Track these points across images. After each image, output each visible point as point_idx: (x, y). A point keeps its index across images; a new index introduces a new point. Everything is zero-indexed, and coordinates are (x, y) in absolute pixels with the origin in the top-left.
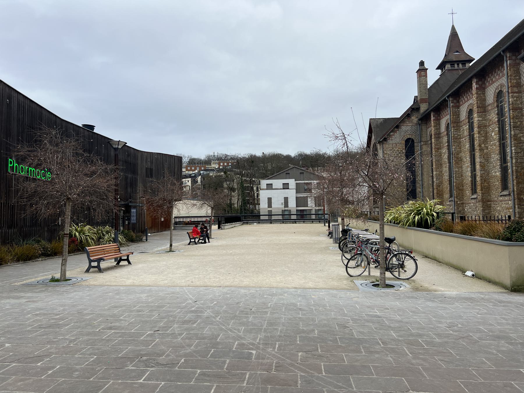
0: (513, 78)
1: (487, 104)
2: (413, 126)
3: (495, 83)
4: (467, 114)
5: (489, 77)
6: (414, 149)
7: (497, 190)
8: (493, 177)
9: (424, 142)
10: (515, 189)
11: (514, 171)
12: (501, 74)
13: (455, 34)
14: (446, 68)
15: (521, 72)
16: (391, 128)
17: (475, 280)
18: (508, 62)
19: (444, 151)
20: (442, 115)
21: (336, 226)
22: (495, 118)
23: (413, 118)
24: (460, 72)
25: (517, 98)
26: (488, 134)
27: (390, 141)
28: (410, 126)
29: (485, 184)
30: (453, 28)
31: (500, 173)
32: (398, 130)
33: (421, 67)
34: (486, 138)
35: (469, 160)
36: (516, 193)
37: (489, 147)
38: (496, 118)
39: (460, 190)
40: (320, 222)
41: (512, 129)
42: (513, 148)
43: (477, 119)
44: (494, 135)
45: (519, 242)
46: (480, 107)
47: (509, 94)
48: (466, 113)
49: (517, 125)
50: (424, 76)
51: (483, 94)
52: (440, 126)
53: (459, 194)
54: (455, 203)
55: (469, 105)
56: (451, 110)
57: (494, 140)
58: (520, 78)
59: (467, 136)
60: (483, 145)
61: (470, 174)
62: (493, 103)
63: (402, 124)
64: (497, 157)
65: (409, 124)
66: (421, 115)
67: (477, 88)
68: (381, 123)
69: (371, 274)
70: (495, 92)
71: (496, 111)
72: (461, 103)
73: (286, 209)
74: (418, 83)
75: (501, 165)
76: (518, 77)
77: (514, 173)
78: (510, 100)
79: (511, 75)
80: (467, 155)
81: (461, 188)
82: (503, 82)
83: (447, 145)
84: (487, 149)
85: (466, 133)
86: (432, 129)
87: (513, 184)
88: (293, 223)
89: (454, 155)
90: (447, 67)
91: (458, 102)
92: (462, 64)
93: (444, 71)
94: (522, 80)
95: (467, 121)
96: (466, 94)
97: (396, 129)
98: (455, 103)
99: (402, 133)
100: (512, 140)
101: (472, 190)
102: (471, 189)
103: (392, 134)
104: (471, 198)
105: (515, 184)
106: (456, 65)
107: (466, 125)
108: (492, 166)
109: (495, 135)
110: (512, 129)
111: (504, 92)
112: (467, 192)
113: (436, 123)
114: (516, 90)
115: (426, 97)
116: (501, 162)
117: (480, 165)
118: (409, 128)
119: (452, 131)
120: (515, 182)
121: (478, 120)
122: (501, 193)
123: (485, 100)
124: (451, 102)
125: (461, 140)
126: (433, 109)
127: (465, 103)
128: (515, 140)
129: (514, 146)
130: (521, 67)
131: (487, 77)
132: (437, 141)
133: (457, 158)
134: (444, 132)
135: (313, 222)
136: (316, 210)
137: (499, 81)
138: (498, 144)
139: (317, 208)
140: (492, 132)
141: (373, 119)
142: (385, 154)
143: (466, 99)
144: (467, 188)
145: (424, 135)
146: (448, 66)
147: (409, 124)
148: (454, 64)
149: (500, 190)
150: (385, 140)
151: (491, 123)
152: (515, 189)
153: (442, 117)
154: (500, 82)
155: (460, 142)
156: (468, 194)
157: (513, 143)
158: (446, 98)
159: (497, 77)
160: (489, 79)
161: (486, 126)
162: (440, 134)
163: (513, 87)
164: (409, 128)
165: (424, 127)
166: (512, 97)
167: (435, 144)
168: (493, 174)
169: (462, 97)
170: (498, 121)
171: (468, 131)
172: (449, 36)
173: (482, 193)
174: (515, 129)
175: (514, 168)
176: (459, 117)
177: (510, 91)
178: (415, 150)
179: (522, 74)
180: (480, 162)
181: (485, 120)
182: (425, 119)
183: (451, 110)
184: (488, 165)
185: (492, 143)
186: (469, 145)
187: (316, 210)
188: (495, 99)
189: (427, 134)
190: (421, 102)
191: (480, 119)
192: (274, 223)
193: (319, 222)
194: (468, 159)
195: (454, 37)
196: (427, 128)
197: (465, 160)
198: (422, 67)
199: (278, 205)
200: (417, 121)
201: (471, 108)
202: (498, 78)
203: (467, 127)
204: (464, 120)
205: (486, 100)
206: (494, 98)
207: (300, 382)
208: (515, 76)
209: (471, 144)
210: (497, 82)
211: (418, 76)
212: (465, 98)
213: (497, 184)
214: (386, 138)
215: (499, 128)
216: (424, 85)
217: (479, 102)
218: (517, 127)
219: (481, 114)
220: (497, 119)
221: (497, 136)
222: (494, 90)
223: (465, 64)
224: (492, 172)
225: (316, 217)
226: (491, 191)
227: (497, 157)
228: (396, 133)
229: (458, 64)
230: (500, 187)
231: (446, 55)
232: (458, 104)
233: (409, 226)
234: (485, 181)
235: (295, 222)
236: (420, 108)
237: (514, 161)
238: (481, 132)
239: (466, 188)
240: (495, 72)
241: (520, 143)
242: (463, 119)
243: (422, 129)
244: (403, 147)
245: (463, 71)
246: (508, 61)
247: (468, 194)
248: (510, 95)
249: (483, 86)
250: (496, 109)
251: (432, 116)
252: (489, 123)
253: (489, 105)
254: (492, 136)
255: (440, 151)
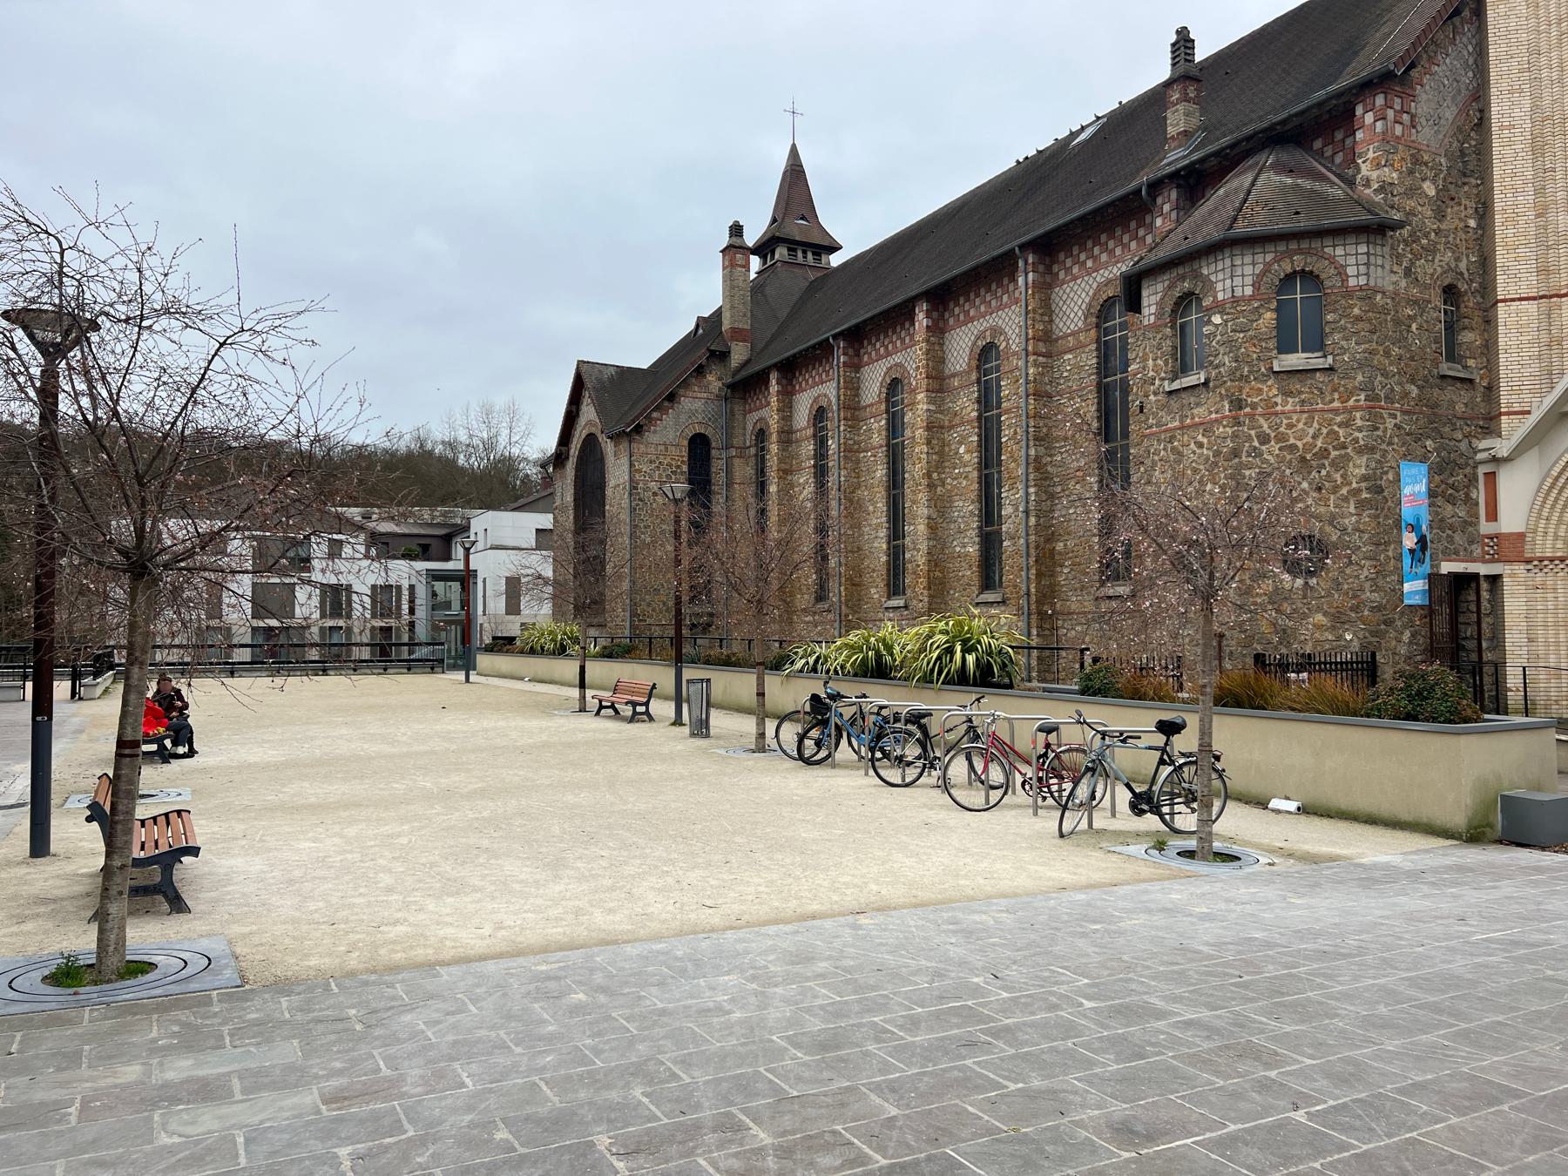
0: (1038, 317)
1: (947, 371)
2: (709, 402)
3: (975, 323)
4: (884, 390)
5: (957, 304)
6: (709, 466)
7: (964, 590)
8: (956, 555)
9: (737, 448)
10: (1033, 590)
11: (1032, 545)
12: (994, 303)
13: (798, 168)
14: (777, 256)
15: (1054, 306)
16: (655, 400)
17: (1303, 818)
18: (1031, 275)
19: (801, 481)
20: (800, 384)
21: (705, 685)
22: (969, 409)
23: (710, 378)
24: (812, 276)
25: (1043, 367)
26: (947, 449)
27: (651, 435)
28: (703, 401)
29: (937, 573)
30: (794, 152)
31: (977, 547)
32: (672, 408)
33: (734, 239)
34: (941, 458)
35: (885, 509)
36: (1033, 598)
37: (949, 480)
38: (973, 410)
39: (853, 585)
40: (409, 669)
41: (1031, 443)
42: (1032, 490)
43: (925, 407)
44: (966, 453)
45: (1440, 722)
46: (932, 378)
47: (1027, 355)
48: (881, 386)
49: (1042, 435)
50: (744, 266)
51: (939, 344)
52: (791, 412)
53: (852, 594)
54: (843, 618)
55: (891, 367)
56: (842, 373)
57: (965, 466)
58: (1051, 321)
59: (881, 446)
60: (935, 475)
61: (885, 546)
62: (968, 373)
63: (682, 391)
64: (971, 507)
65: (699, 395)
66: (734, 375)
67: (927, 326)
68: (611, 379)
69: (1096, 825)
70: (974, 344)
71: (974, 392)
72: (866, 358)
73: (214, 623)
74: (724, 281)
75: (980, 528)
76: (1047, 318)
77: (1032, 551)
78: (1031, 371)
79: (1034, 311)
80: (878, 495)
81: (857, 579)
82: (1000, 323)
83: (814, 466)
84: (943, 485)
85: (878, 439)
86: (771, 415)
87: (1028, 578)
88: (317, 675)
89: (845, 492)
90: (780, 254)
91: (858, 355)
92: (814, 254)
93: (769, 264)
94: (1054, 327)
95: (883, 407)
96: (882, 337)
97: (666, 404)
98: (850, 357)
99: (683, 418)
100: (1031, 470)
101: (888, 585)
102: (885, 582)
103: (655, 415)
104: (886, 605)
105: (1033, 577)
106: (800, 254)
107: (879, 418)
108: (956, 530)
109: (968, 451)
110: (1031, 443)
111: (1001, 348)
112: (873, 591)
113: (783, 402)
114: (1042, 348)
115: (746, 327)
116: (981, 521)
117: (928, 523)
118: (699, 405)
119: (842, 428)
120: (1033, 571)
121: (928, 410)
122: (977, 596)
123: (942, 361)
124: (841, 350)
125: (862, 455)
126: (781, 362)
127: (877, 361)
128: (1037, 469)
129: (1035, 485)
130: (1054, 295)
131: (951, 305)
132: (784, 450)
133: (851, 501)
134: (805, 429)
135: (385, 669)
136: (322, 629)
137: (987, 318)
138: (975, 474)
139: (330, 623)
140: (960, 443)
141: (588, 362)
142: (636, 471)
143: (882, 349)
144: (874, 581)
145: (738, 431)
146: (781, 252)
147: (699, 395)
148: (795, 250)
149: (975, 590)
150: (639, 429)
151: (957, 420)
152: (1033, 590)
153: (800, 386)
154: (991, 321)
155: (858, 462)
156: (876, 596)
157: (1031, 477)
158: (831, 340)
159: (983, 308)
160: (957, 310)
161: (942, 427)
162: (790, 432)
163: (1038, 340)
164: (699, 405)
165: (738, 408)
166: (1036, 364)
167: (778, 459)
168: (958, 549)
169: (870, 343)
170: (979, 418)
171: (884, 433)
172: (785, 173)
173: (930, 596)
174: (1037, 443)
175: (1032, 538)
176: (857, 395)
177: (1030, 348)
178: (713, 470)
179: (1057, 312)
180: (929, 518)
181: (941, 412)
182: (746, 387)
183: (842, 373)
184: (944, 525)
185: (957, 471)
186: (884, 471)
187: (322, 629)
188: (974, 363)
189: (745, 429)
190: (733, 338)
191: (932, 407)
192: (244, 674)
193: (406, 671)
194: (882, 506)
195: (795, 175)
196: (744, 411)
197: (871, 508)
198: (737, 241)
199: (1469, 634)
200: (720, 388)
201: (898, 376)
202: (986, 312)
203: (883, 422)
204: (872, 405)
205: (947, 361)
206: (969, 359)
207: (1317, 1165)
208: (1042, 315)
209: (889, 469)
210: (981, 321)
211: (727, 263)
212: (878, 346)
213: (969, 574)
214: (642, 426)
215: (979, 435)
216: (741, 292)
217: (930, 363)
218: (1042, 439)
219: (934, 395)
220: (975, 414)
221: (975, 454)
222: (973, 338)
223: (819, 255)
224: (955, 543)
225: (372, 654)
226: (948, 592)
227: (971, 507)
228: (667, 414)
229: (804, 252)
230: (976, 581)
231: (774, 220)
232: (856, 360)
233: (943, 683)
234: (936, 565)
235: (325, 672)
236: (729, 352)
237: (1032, 521)
238: (933, 442)
239: (870, 580)
240: (977, 295)
241: (1045, 479)
242: (868, 402)
243: (732, 413)
244: (684, 456)
245: (819, 275)
246: (1031, 274)
247: (876, 596)
248: (1031, 358)
249: (941, 324)
250: (976, 389)
251: (774, 382)
252: (950, 421)
253: (953, 375)
254: (957, 453)
255: (789, 478)
